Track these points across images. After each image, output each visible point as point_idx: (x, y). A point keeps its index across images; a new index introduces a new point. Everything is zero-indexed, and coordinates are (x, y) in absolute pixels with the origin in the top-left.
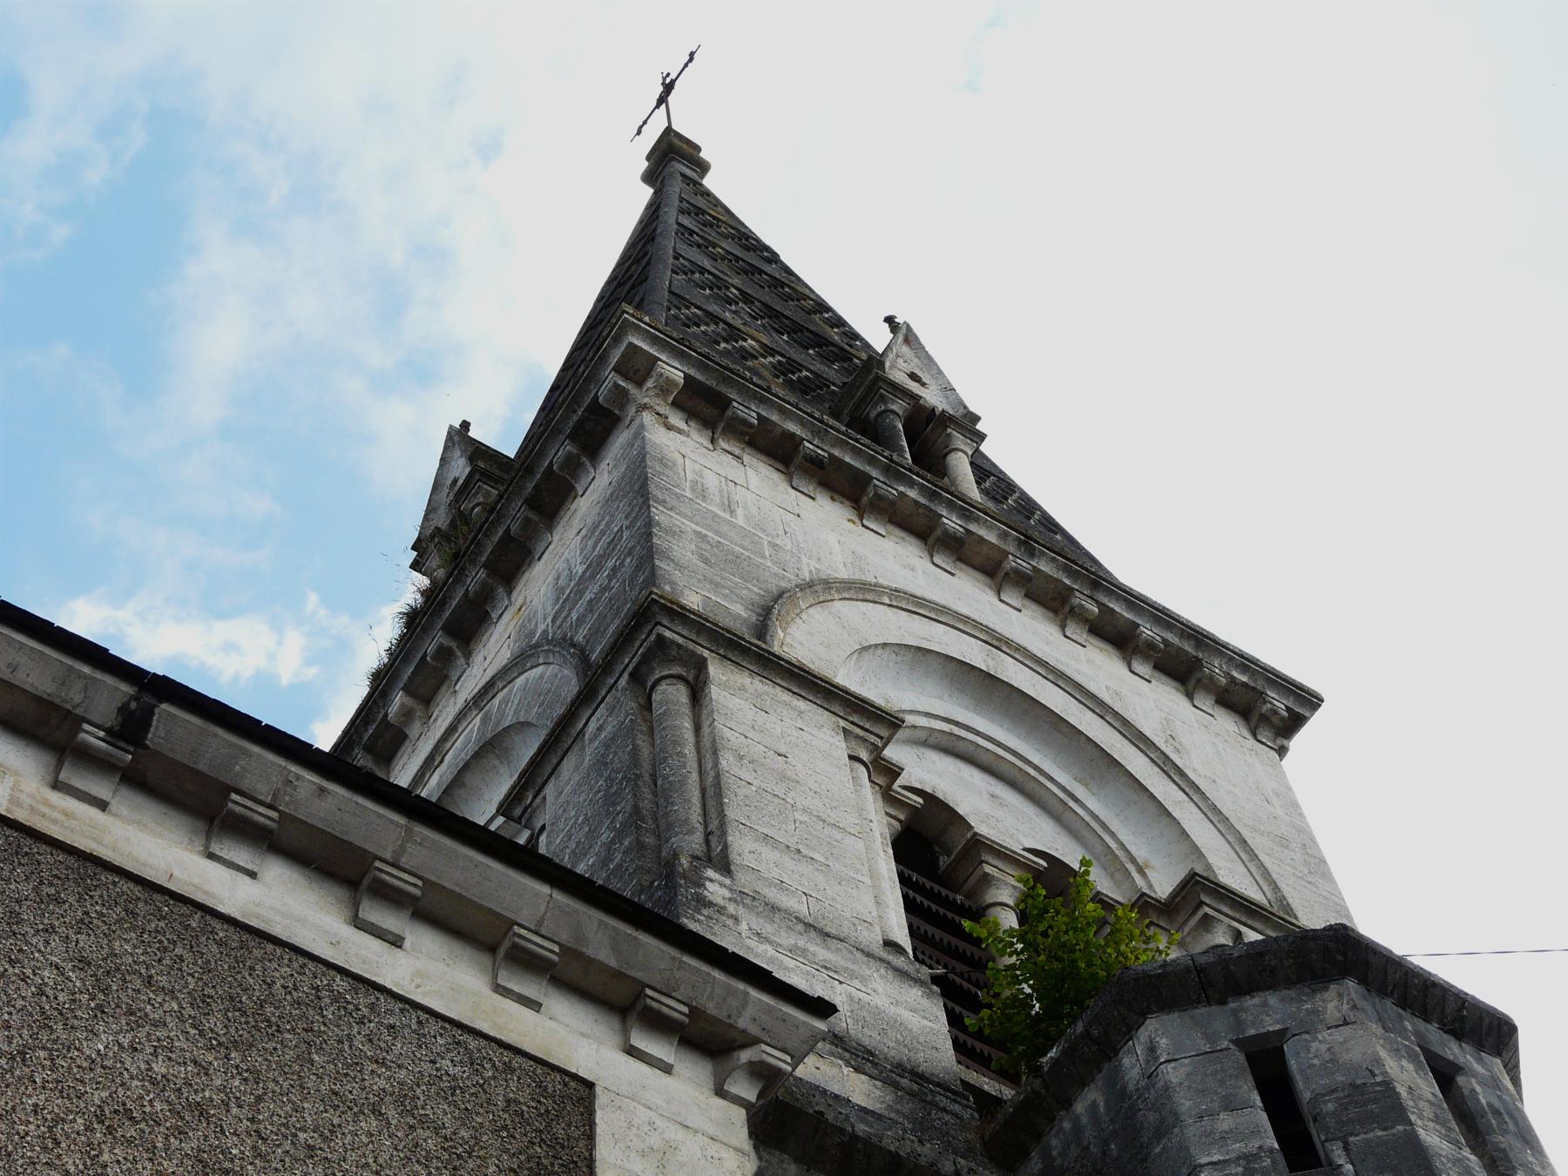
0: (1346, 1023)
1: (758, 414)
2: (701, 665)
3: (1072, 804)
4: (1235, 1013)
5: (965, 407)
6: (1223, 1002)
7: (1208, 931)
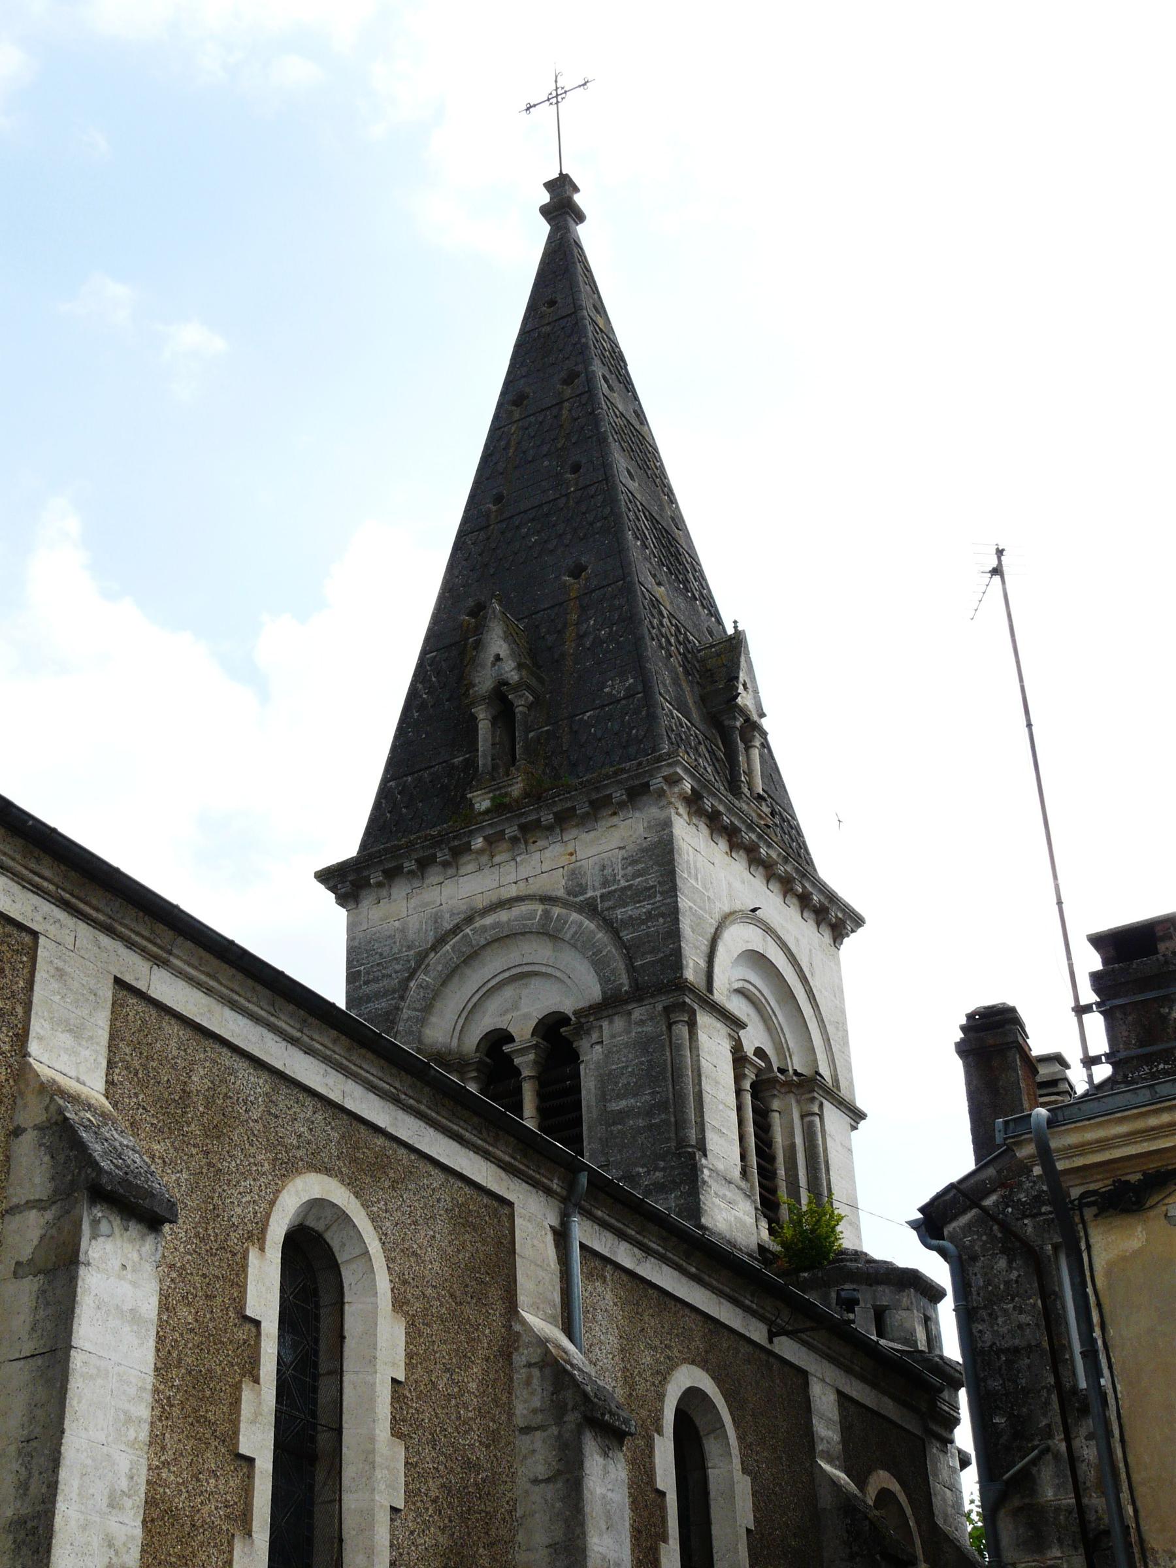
0: (908, 1309)
1: (712, 803)
2: (693, 1013)
3: (773, 1018)
4: (875, 1291)
5: (762, 709)
6: (871, 1285)
7: (812, 1103)
